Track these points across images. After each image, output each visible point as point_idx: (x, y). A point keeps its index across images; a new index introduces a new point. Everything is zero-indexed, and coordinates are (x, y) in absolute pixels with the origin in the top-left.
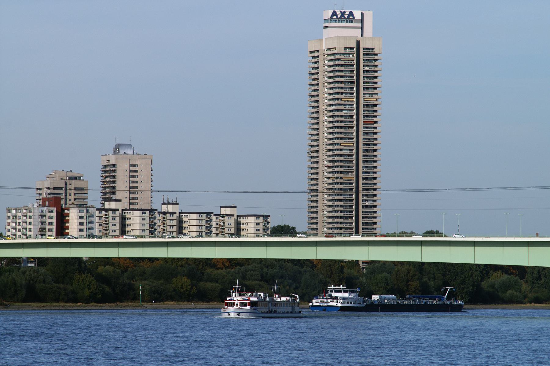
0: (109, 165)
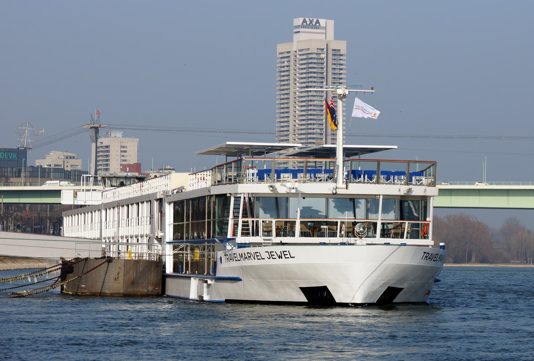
0: (101, 147)
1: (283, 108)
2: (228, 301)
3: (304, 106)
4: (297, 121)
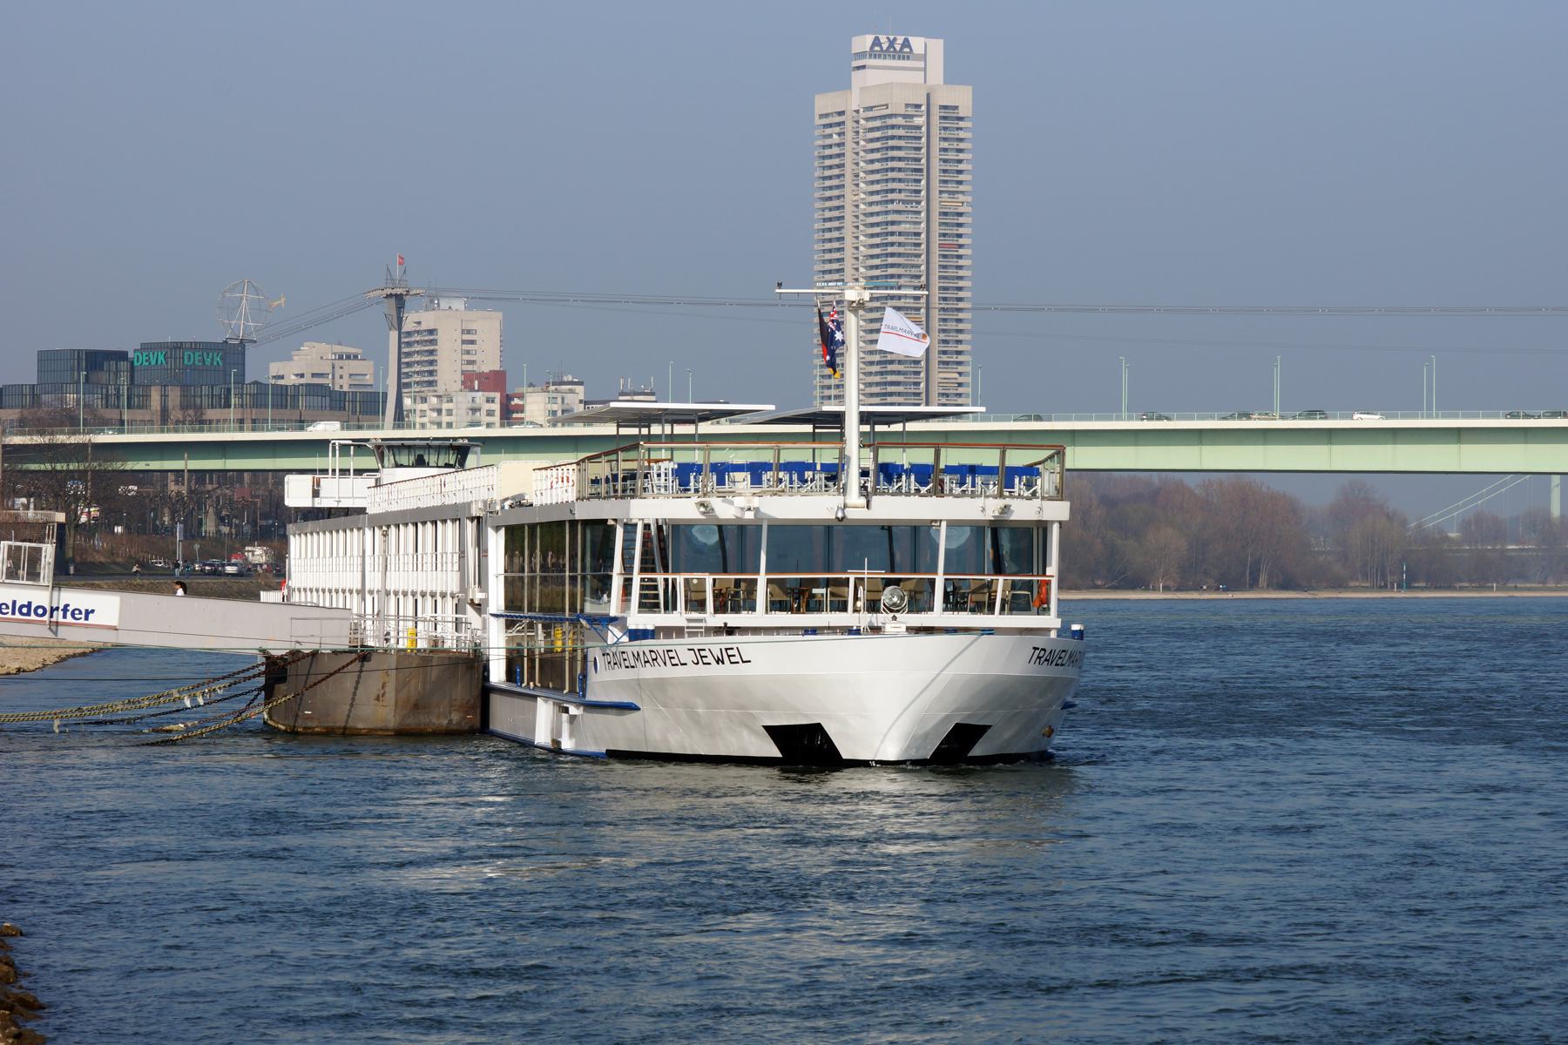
0: (418, 332)
1: (830, 240)
2: (615, 755)
3: (877, 235)
4: (862, 270)
